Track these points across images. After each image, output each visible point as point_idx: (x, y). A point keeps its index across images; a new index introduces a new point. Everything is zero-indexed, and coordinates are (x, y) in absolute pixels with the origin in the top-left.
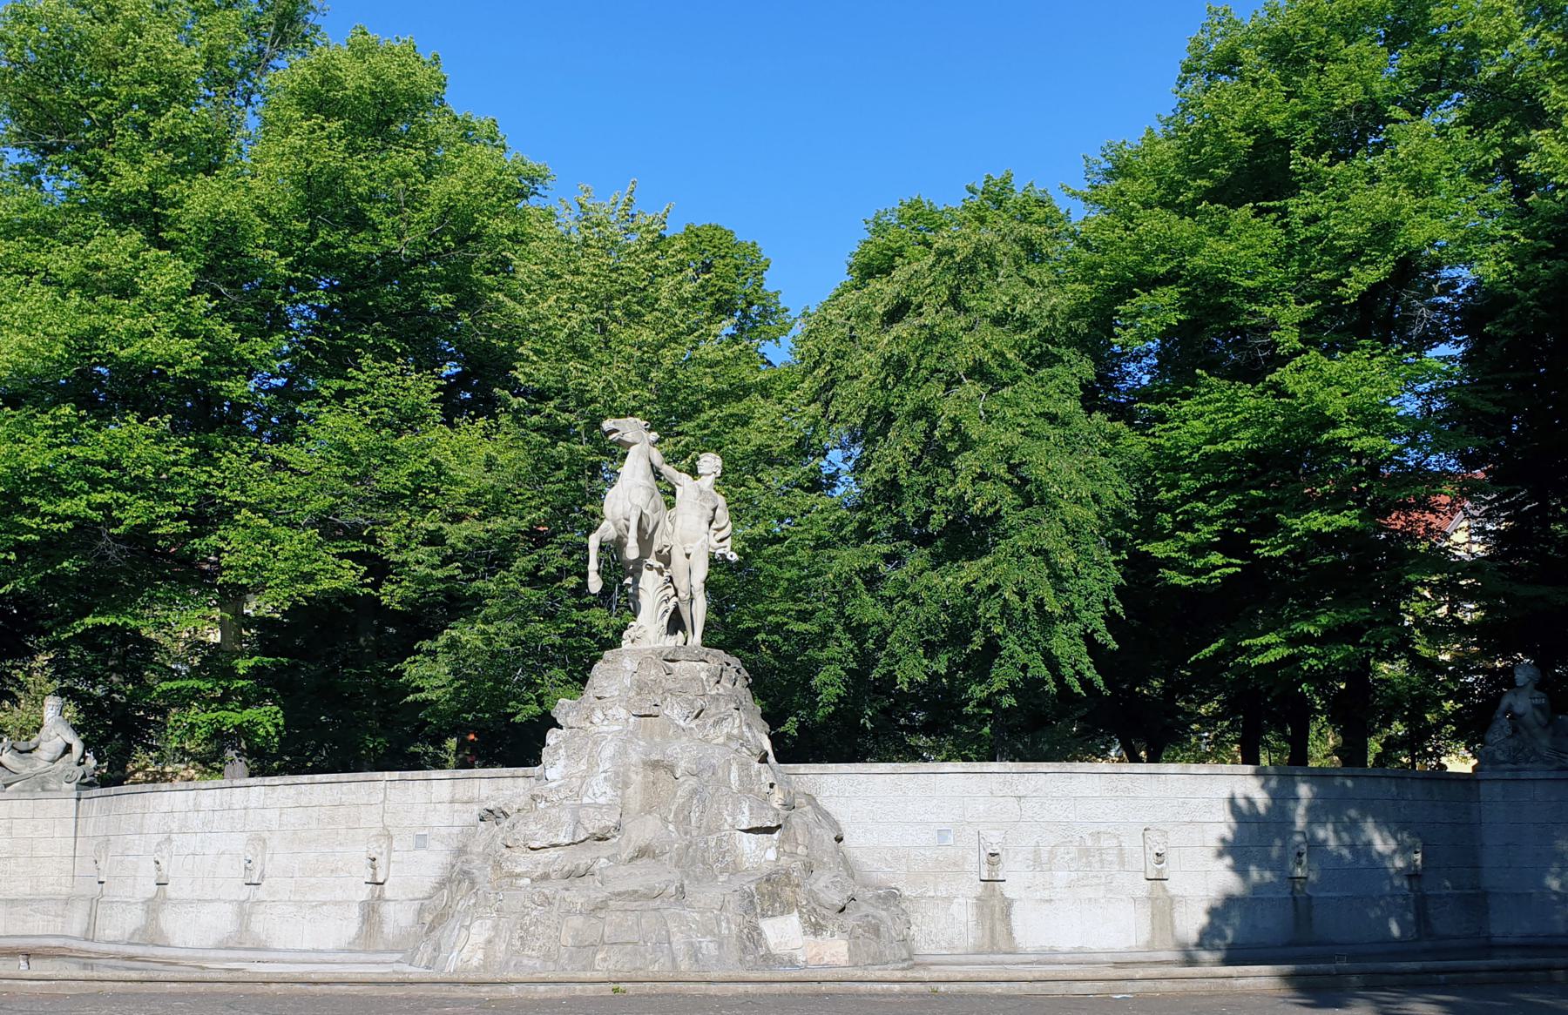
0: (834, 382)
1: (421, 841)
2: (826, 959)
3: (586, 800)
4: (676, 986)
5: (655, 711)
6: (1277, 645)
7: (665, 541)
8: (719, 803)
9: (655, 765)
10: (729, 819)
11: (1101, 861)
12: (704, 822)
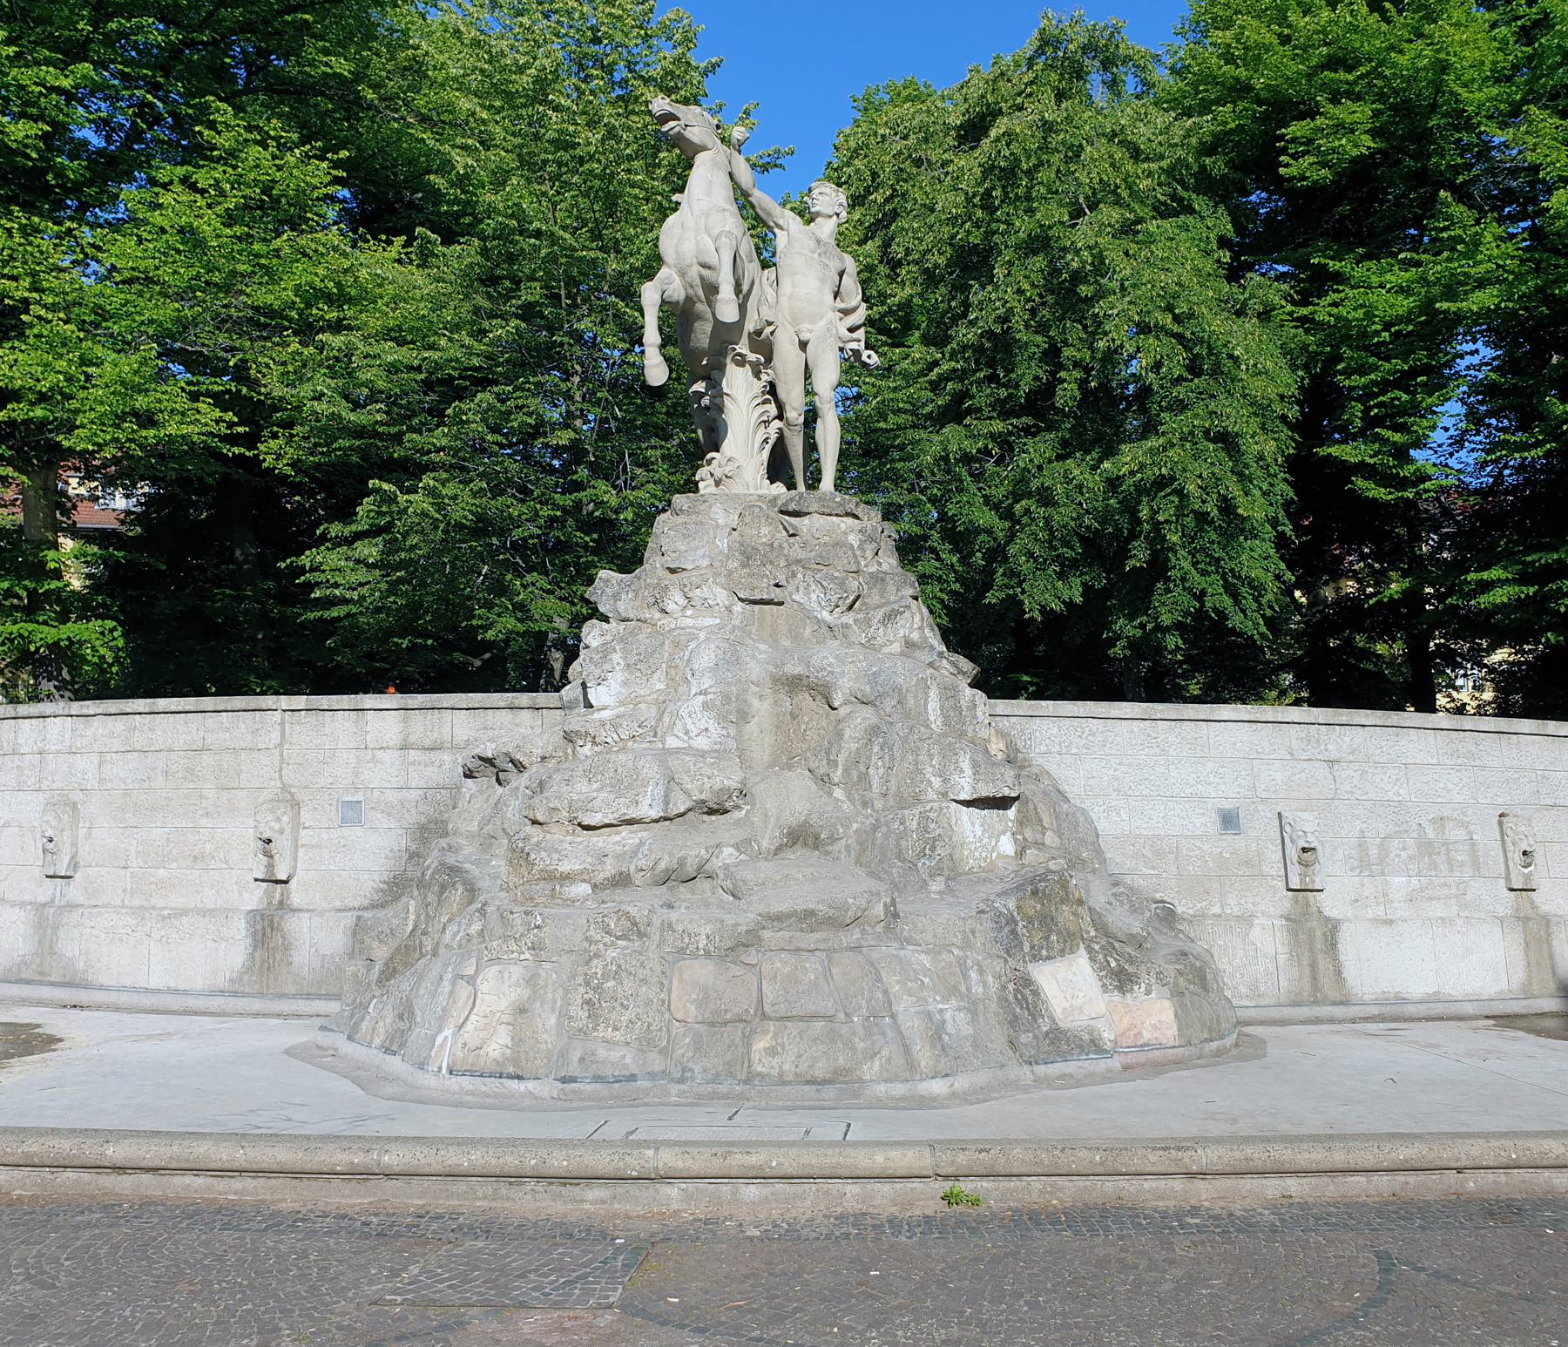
0: (894, 215)
1: (352, 813)
2: (1147, 1035)
3: (672, 742)
4: (1110, 1186)
5: (776, 594)
6: (1502, 583)
7: (767, 314)
8: (916, 751)
9: (794, 684)
10: (937, 782)
11: (1449, 861)
12: (893, 786)
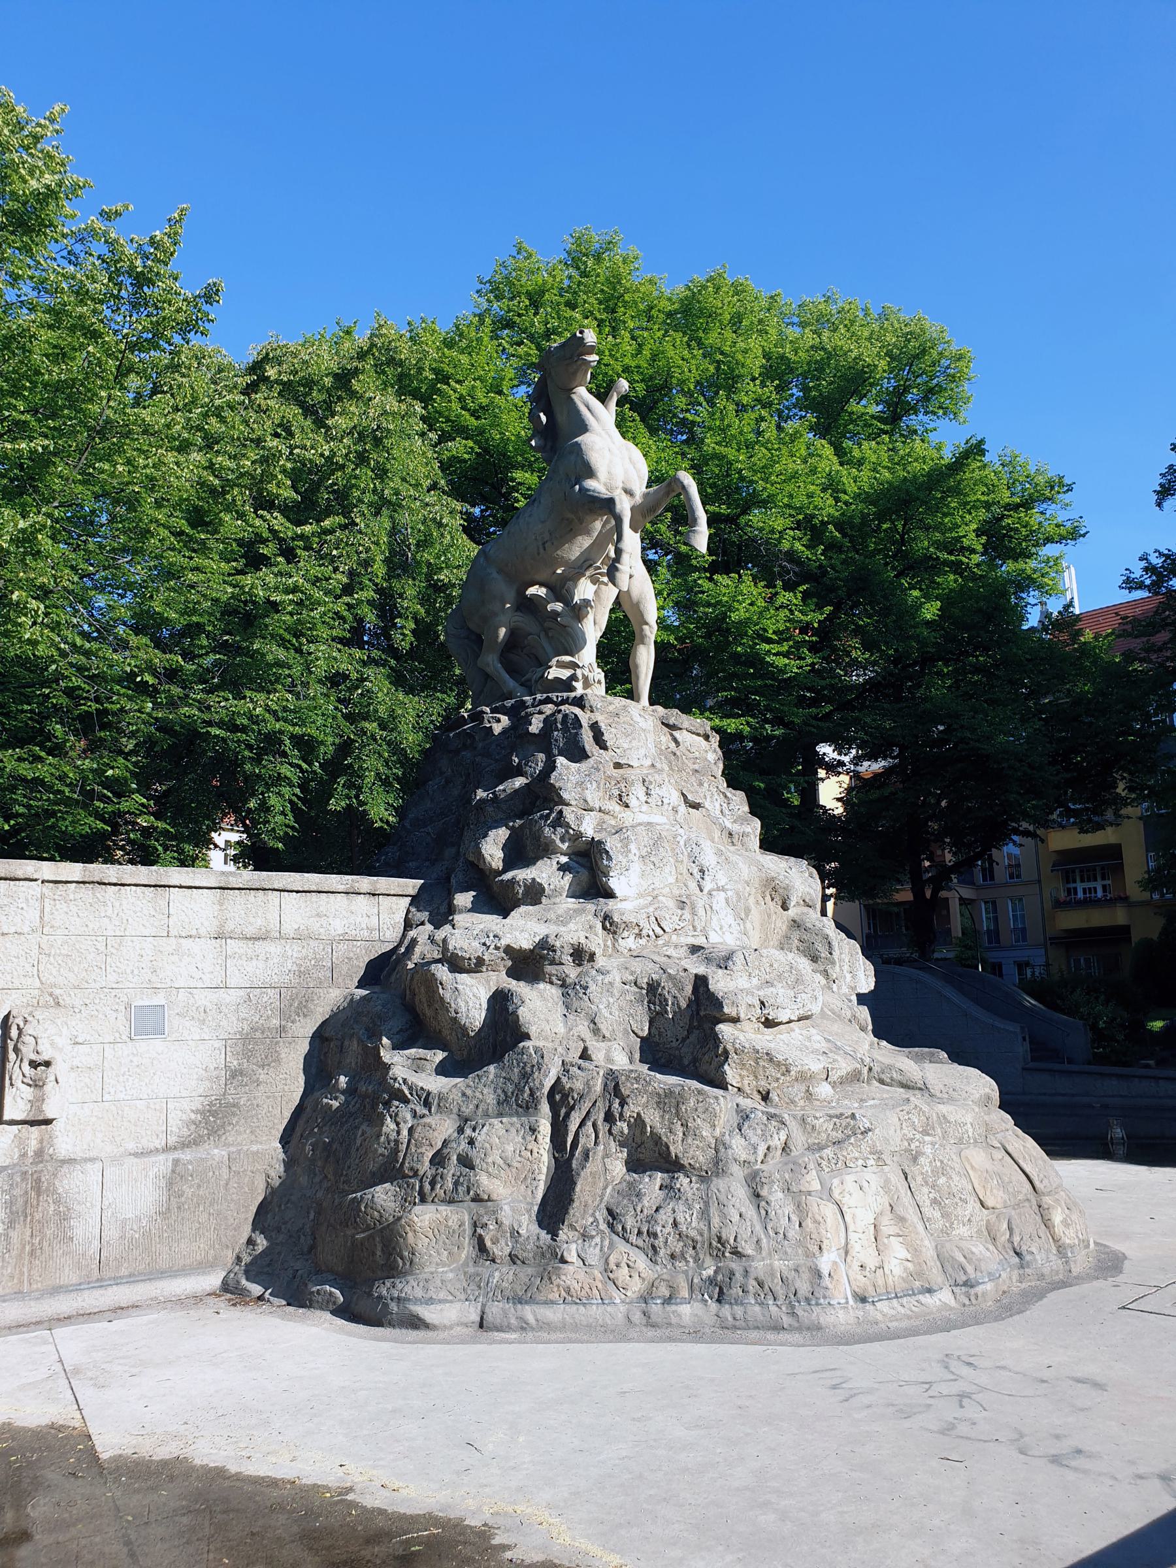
1: (148, 1023)
